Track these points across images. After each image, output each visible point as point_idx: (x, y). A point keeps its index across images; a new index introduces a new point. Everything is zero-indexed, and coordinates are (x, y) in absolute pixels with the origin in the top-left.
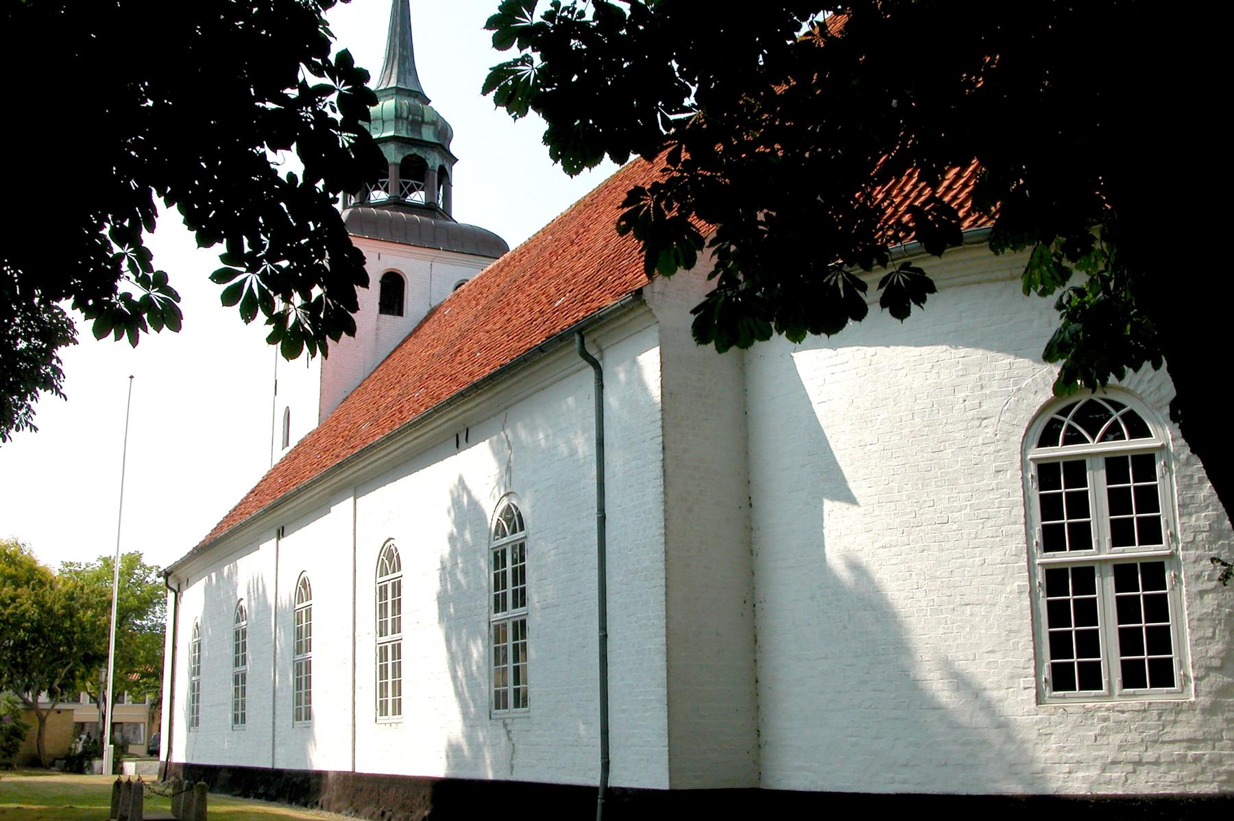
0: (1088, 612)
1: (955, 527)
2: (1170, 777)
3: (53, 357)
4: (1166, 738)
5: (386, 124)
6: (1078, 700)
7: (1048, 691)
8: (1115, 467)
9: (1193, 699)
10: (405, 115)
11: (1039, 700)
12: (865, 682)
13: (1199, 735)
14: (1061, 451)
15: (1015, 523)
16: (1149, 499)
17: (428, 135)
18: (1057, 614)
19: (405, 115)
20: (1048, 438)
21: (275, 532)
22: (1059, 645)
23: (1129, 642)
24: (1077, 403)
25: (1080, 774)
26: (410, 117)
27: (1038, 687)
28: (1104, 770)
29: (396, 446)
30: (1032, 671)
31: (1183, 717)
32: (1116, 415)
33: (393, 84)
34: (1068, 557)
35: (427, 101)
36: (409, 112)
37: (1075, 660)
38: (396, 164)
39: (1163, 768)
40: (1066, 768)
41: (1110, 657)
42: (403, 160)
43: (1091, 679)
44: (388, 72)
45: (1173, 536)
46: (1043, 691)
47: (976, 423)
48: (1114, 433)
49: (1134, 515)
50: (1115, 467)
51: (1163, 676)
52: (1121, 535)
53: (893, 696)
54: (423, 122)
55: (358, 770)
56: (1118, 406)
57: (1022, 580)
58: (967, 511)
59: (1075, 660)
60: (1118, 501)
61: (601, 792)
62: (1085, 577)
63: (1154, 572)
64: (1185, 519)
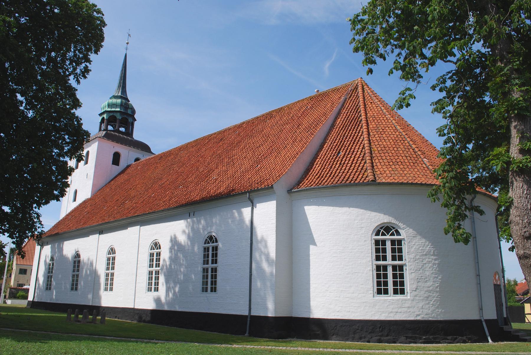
0: (386, 276)
1: (354, 253)
2: (404, 316)
4: (403, 307)
5: (117, 107)
6: (383, 297)
7: (376, 294)
8: (393, 242)
9: (409, 298)
10: (123, 105)
11: (374, 296)
12: (327, 290)
13: (410, 306)
14: (380, 237)
15: (369, 254)
16: (400, 250)
17: (129, 112)
18: (378, 276)
19: (123, 105)
20: (377, 234)
21: (99, 232)
22: (379, 284)
23: (395, 284)
24: (384, 226)
25: (383, 315)
26: (125, 106)
27: (373, 294)
28: (389, 314)
29: (163, 213)
30: (372, 290)
31: (407, 302)
33: (120, 94)
34: (381, 263)
35: (129, 101)
36: (125, 104)
38: (119, 119)
39: (402, 314)
40: (380, 313)
42: (121, 118)
44: (118, 90)
45: (405, 260)
47: (360, 229)
48: (392, 234)
49: (397, 254)
50: (393, 242)
51: (402, 292)
52: (394, 258)
53: (335, 294)
54: (128, 108)
55: (135, 308)
56: (394, 228)
57: (370, 268)
58: (357, 250)
60: (393, 250)
61: (249, 317)
62: (385, 268)
63: (401, 268)
64: (408, 256)
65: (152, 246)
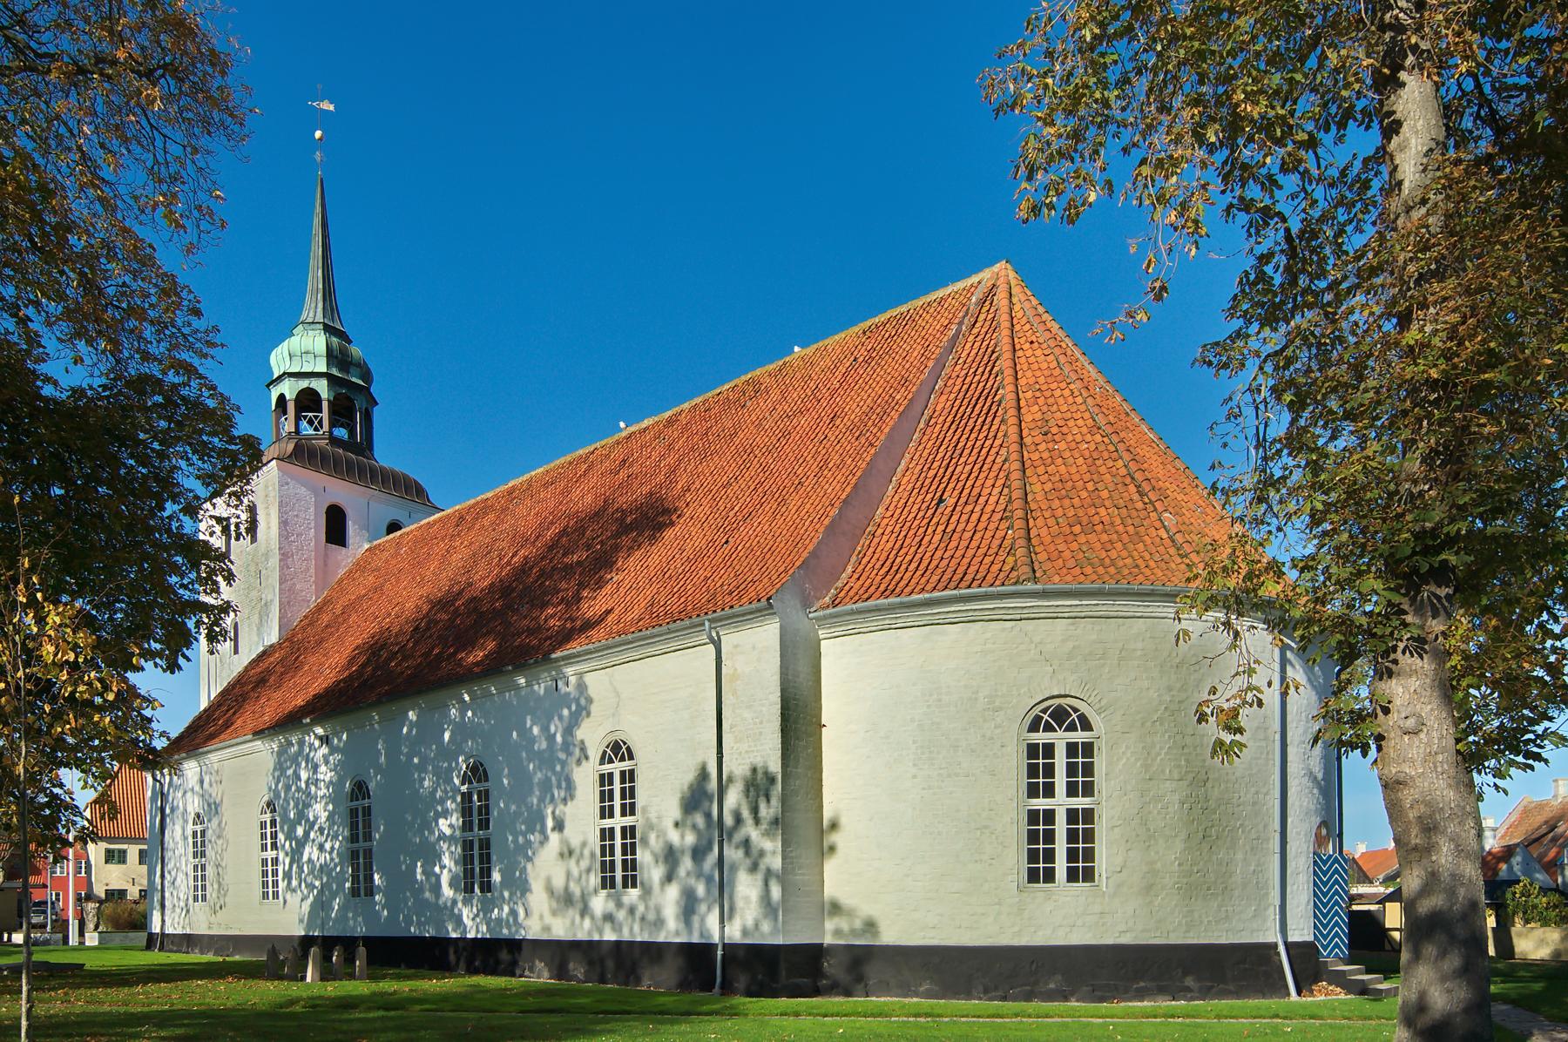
3: (77, 407)
16: (1088, 770)
20: (1034, 727)
22: (1033, 856)
32: (1074, 716)
37: (1041, 865)
41: (1061, 865)
43: (1050, 876)
46: (977, 304)
52: (1072, 791)
59: (1041, 846)
60: (1071, 770)
65: (605, 752)
